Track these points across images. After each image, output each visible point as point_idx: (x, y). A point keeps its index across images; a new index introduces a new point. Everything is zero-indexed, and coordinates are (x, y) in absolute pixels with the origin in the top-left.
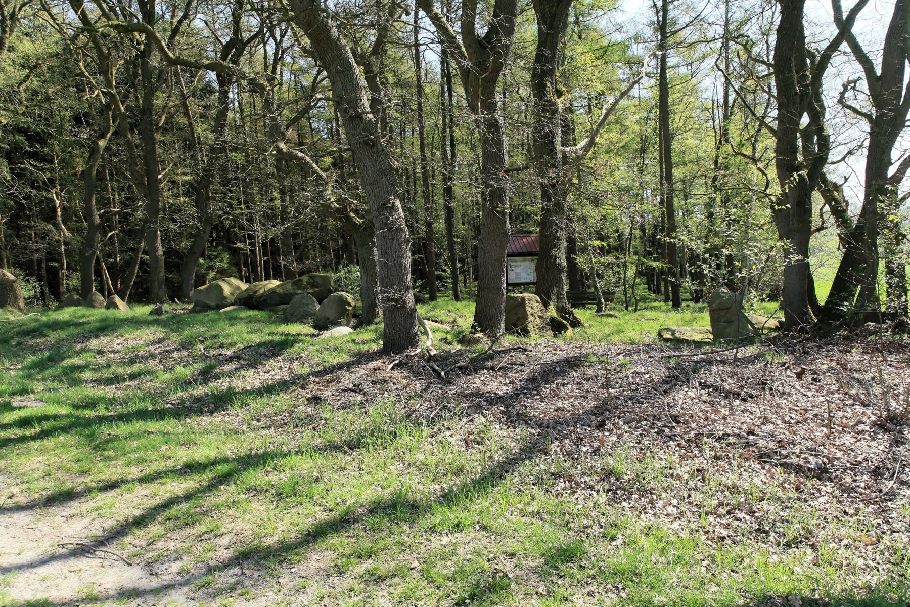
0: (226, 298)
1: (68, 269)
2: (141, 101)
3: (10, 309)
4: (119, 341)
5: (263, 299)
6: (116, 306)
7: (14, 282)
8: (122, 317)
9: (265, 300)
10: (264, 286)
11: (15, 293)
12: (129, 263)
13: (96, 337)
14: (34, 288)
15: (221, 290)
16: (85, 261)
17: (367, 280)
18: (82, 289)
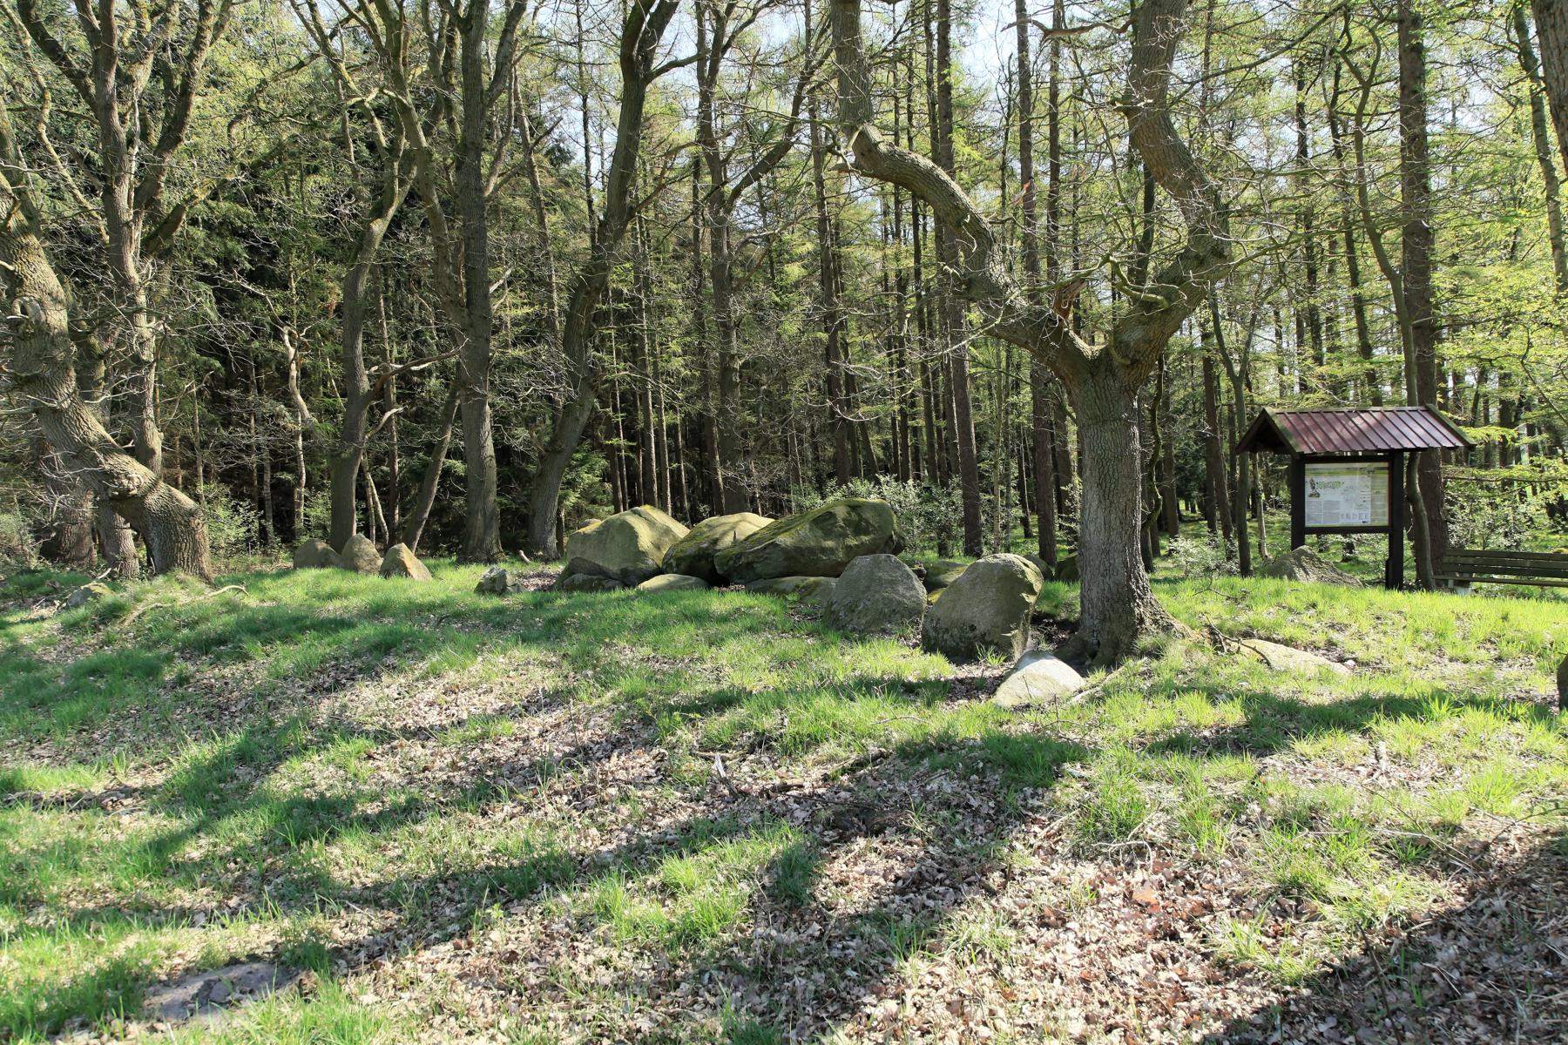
0: (644, 554)
1: (308, 486)
2: (459, 130)
3: (182, 575)
4: (430, 695)
5: (743, 560)
6: (403, 570)
7: (192, 513)
8: (420, 600)
9: (749, 565)
10: (733, 528)
11: (194, 540)
12: (419, 475)
13: (371, 673)
14: (245, 523)
15: (633, 535)
16: (340, 467)
17: (1107, 523)
18: (333, 525)
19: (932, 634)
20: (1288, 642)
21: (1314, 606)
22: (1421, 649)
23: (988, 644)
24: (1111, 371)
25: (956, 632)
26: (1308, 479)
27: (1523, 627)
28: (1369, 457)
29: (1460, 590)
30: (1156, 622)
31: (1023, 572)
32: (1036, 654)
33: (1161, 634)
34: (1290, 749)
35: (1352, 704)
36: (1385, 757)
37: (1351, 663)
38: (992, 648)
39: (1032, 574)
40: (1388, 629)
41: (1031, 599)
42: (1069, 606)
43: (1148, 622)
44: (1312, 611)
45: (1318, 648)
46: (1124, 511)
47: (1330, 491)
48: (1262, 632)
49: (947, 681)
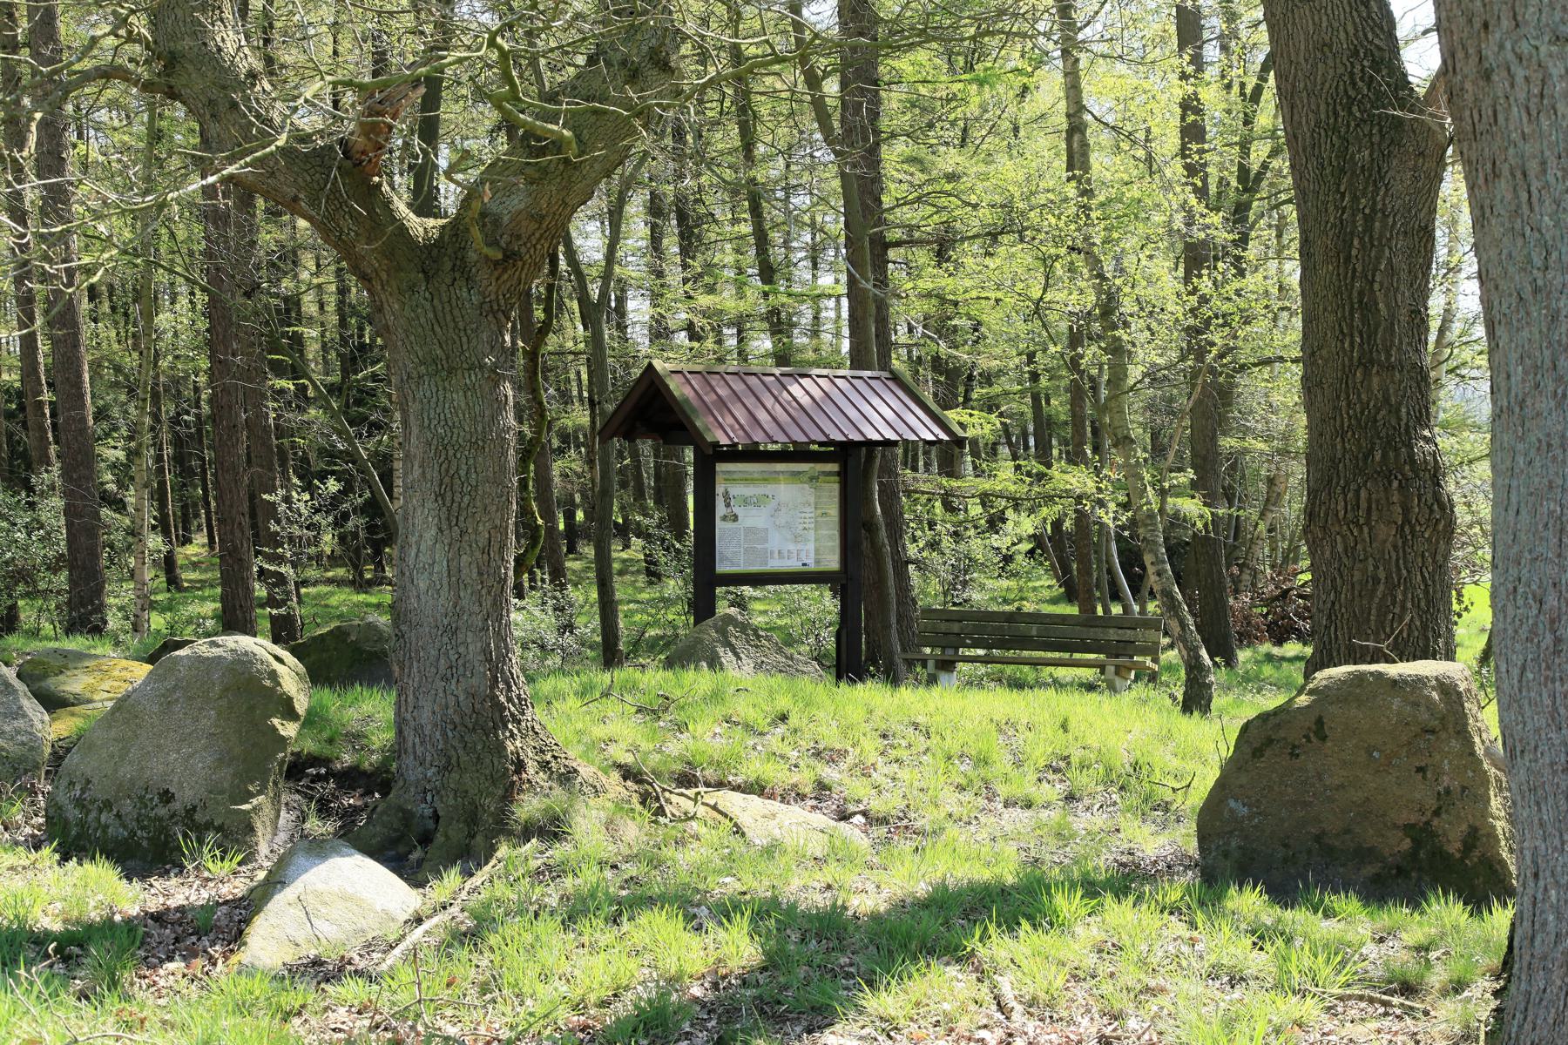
17: (453, 573)
19: (73, 813)
20: (757, 788)
21: (784, 718)
22: (961, 788)
23: (201, 830)
24: (462, 270)
25: (127, 807)
26: (720, 490)
27: (1093, 741)
28: (797, 454)
29: (943, 676)
30: (544, 766)
31: (273, 675)
32: (318, 849)
33: (558, 791)
34: (861, 1010)
35: (925, 905)
36: (1019, 1008)
37: (859, 819)
38: (210, 837)
39: (290, 675)
40: (903, 754)
41: (289, 730)
42: (356, 738)
43: (531, 767)
44: (782, 729)
45: (801, 797)
46: (486, 550)
47: (753, 511)
48: (710, 773)
49: (129, 922)
